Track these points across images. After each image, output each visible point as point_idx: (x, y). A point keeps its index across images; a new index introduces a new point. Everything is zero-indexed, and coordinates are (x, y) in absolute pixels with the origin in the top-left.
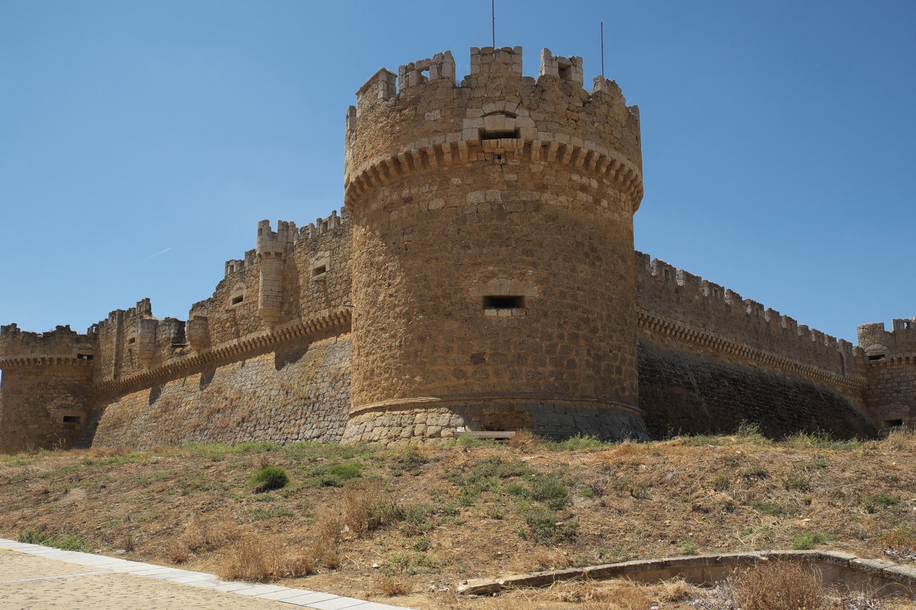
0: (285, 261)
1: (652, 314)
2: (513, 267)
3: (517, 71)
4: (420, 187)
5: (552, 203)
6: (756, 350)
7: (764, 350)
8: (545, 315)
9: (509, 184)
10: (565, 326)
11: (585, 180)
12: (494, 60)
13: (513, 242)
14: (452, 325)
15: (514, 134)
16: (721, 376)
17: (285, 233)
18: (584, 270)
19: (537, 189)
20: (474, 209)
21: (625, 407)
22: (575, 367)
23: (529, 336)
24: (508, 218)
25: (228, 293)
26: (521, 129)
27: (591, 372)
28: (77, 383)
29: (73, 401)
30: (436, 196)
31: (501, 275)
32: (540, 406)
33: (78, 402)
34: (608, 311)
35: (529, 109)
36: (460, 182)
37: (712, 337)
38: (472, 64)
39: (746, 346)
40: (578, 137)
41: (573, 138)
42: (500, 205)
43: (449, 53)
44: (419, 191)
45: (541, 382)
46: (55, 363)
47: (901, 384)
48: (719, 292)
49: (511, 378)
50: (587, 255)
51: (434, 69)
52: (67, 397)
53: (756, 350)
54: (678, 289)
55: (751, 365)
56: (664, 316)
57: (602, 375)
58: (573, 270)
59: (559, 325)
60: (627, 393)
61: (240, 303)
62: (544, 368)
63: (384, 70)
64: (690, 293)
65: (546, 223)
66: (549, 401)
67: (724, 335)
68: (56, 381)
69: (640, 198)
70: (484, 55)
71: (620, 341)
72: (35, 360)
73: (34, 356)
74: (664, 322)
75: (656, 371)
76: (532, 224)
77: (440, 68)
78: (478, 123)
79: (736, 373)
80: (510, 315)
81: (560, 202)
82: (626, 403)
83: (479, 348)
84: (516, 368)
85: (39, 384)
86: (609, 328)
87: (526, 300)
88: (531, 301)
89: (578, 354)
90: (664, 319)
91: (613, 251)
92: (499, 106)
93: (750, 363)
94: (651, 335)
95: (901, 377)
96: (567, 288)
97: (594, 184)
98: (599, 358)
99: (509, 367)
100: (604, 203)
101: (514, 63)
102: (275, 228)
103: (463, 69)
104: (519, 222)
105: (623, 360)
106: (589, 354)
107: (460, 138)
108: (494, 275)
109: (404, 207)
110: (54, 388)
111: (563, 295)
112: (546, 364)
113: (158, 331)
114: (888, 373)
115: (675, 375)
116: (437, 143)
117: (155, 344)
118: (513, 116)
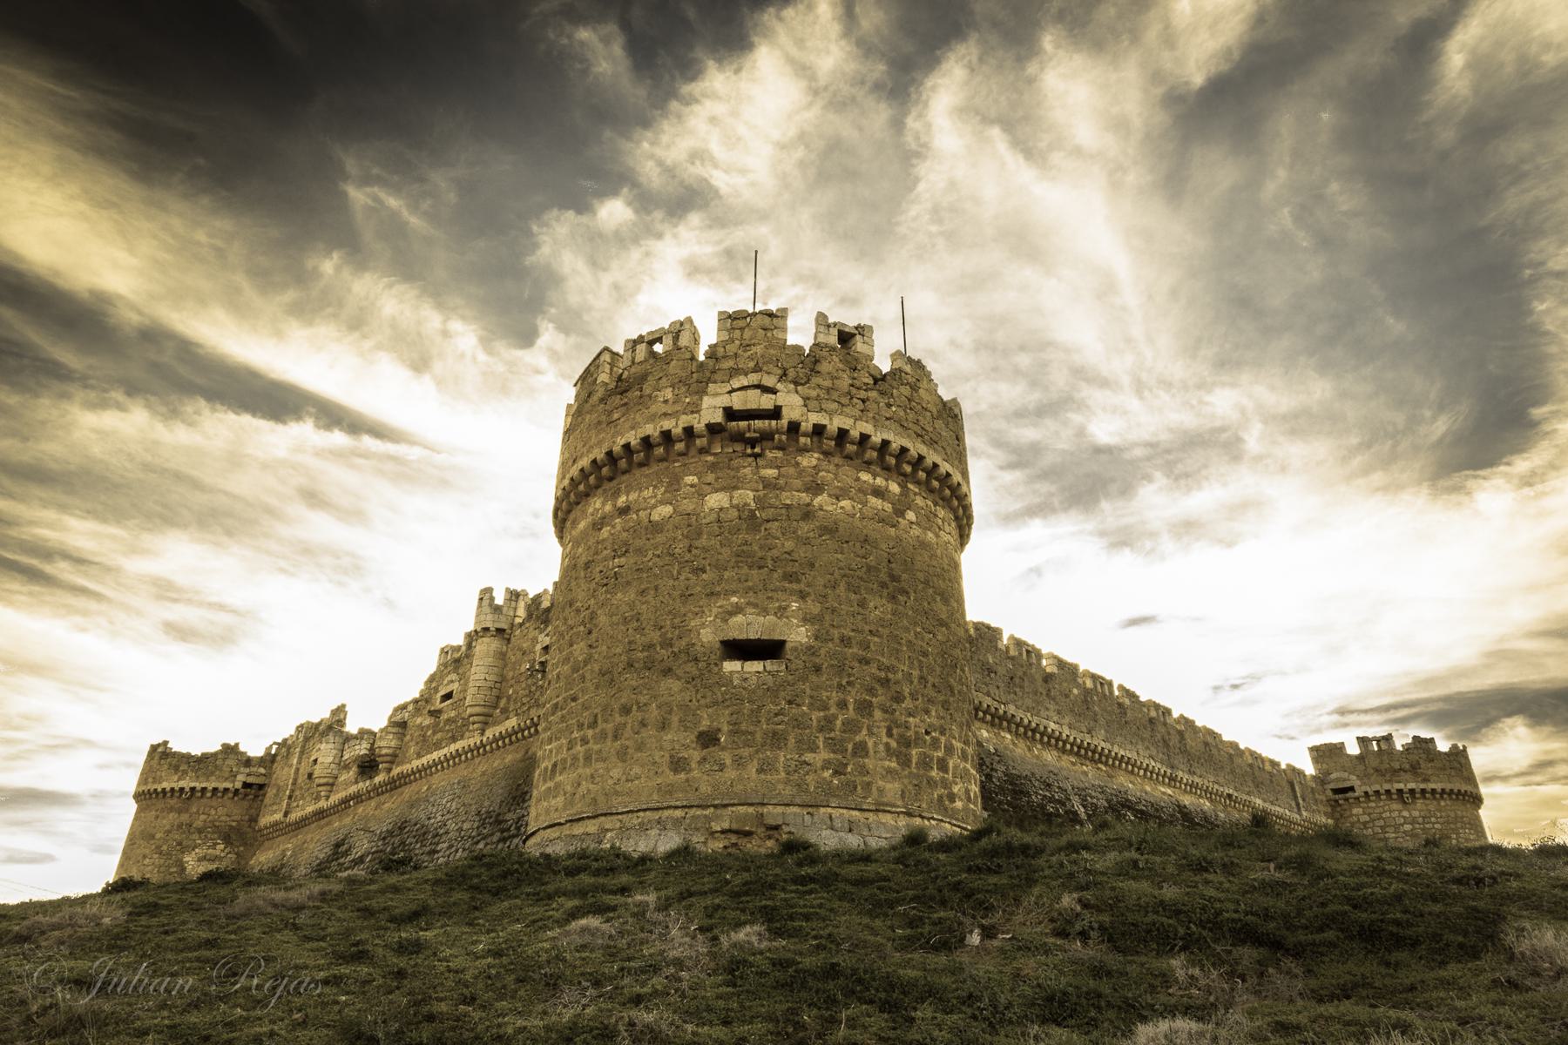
0: (509, 640)
1: (1011, 709)
2: (768, 598)
3: (780, 336)
4: (641, 491)
5: (830, 508)
6: (1169, 771)
7: (1181, 773)
8: (818, 669)
9: (768, 484)
10: (849, 688)
11: (879, 481)
12: (748, 325)
13: (770, 563)
14: (672, 686)
15: (776, 413)
16: (1123, 806)
17: (513, 603)
18: (879, 608)
19: (807, 490)
20: (713, 517)
21: (955, 825)
22: (867, 755)
23: (790, 703)
24: (763, 529)
25: (436, 690)
26: (783, 408)
27: (894, 765)
28: (234, 824)
29: (223, 851)
30: (662, 503)
31: (749, 610)
32: (807, 818)
33: (230, 853)
34: (921, 670)
35: (796, 383)
36: (696, 480)
37: (1103, 749)
38: (719, 330)
39: (1153, 764)
40: (867, 422)
41: (858, 423)
42: (752, 512)
43: (689, 320)
44: (639, 496)
45: (809, 778)
46: (209, 795)
47: (1387, 829)
48: (1106, 687)
49: (760, 771)
50: (883, 585)
51: (668, 340)
52: (215, 844)
53: (1169, 771)
54: (1048, 678)
55: (1164, 793)
56: (1029, 714)
57: (915, 771)
58: (862, 604)
59: (840, 686)
60: (959, 804)
61: (449, 702)
62: (814, 755)
63: (606, 349)
64: (1065, 685)
65: (820, 536)
66: (822, 810)
67: (1120, 747)
68: (205, 821)
69: (969, 525)
70: (736, 319)
71: (943, 718)
72: (182, 789)
73: (182, 784)
74: (1030, 722)
75: (1022, 792)
76: (798, 537)
77: (676, 337)
78: (724, 401)
79: (1144, 802)
80: (761, 668)
81: (842, 508)
82: (957, 819)
83: (712, 722)
84: (768, 753)
85: (180, 826)
86: (923, 695)
87: (788, 646)
88: (795, 649)
89: (871, 733)
90: (1030, 719)
91: (926, 583)
92: (753, 378)
93: (1163, 790)
94: (1012, 740)
95: (1383, 819)
96: (853, 630)
97: (894, 488)
98: (906, 743)
99: (757, 752)
100: (911, 515)
101: (776, 328)
102: (499, 599)
103: (800, 334)
104: (779, 534)
105: (950, 750)
106: (889, 734)
107: (696, 421)
108: (738, 610)
109: (618, 520)
110: (200, 831)
111: (845, 641)
112: (818, 748)
113: (346, 746)
114: (1364, 813)
115: (1051, 800)
116: (666, 428)
117: (339, 764)
118: (773, 391)
